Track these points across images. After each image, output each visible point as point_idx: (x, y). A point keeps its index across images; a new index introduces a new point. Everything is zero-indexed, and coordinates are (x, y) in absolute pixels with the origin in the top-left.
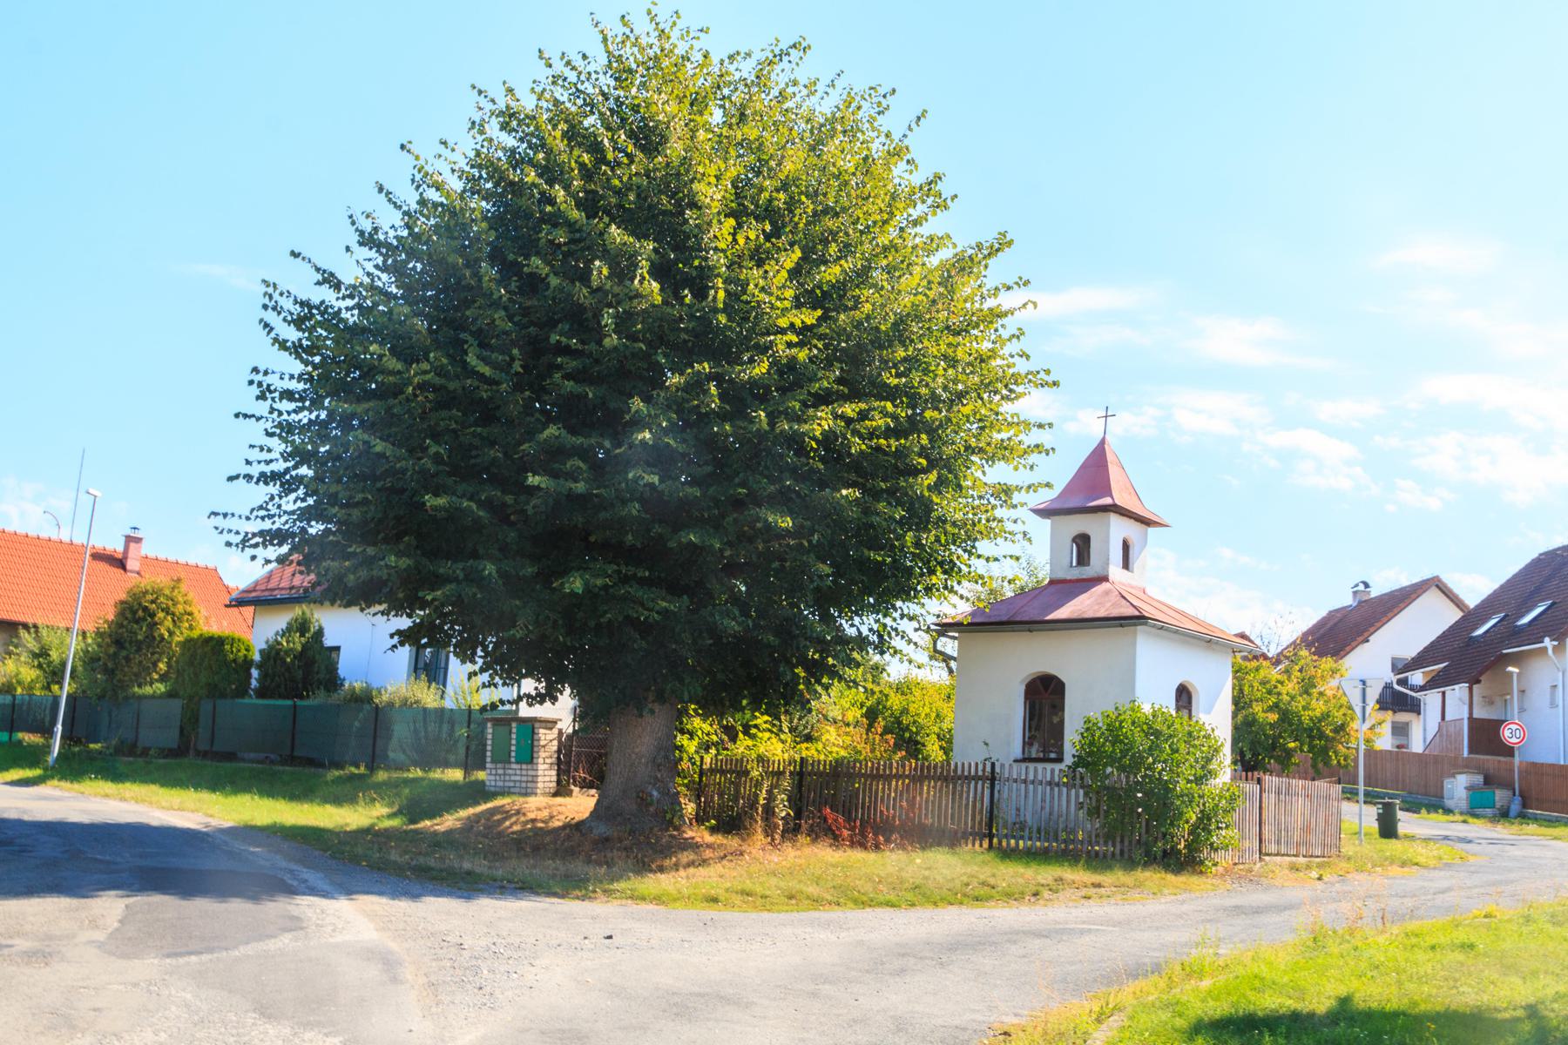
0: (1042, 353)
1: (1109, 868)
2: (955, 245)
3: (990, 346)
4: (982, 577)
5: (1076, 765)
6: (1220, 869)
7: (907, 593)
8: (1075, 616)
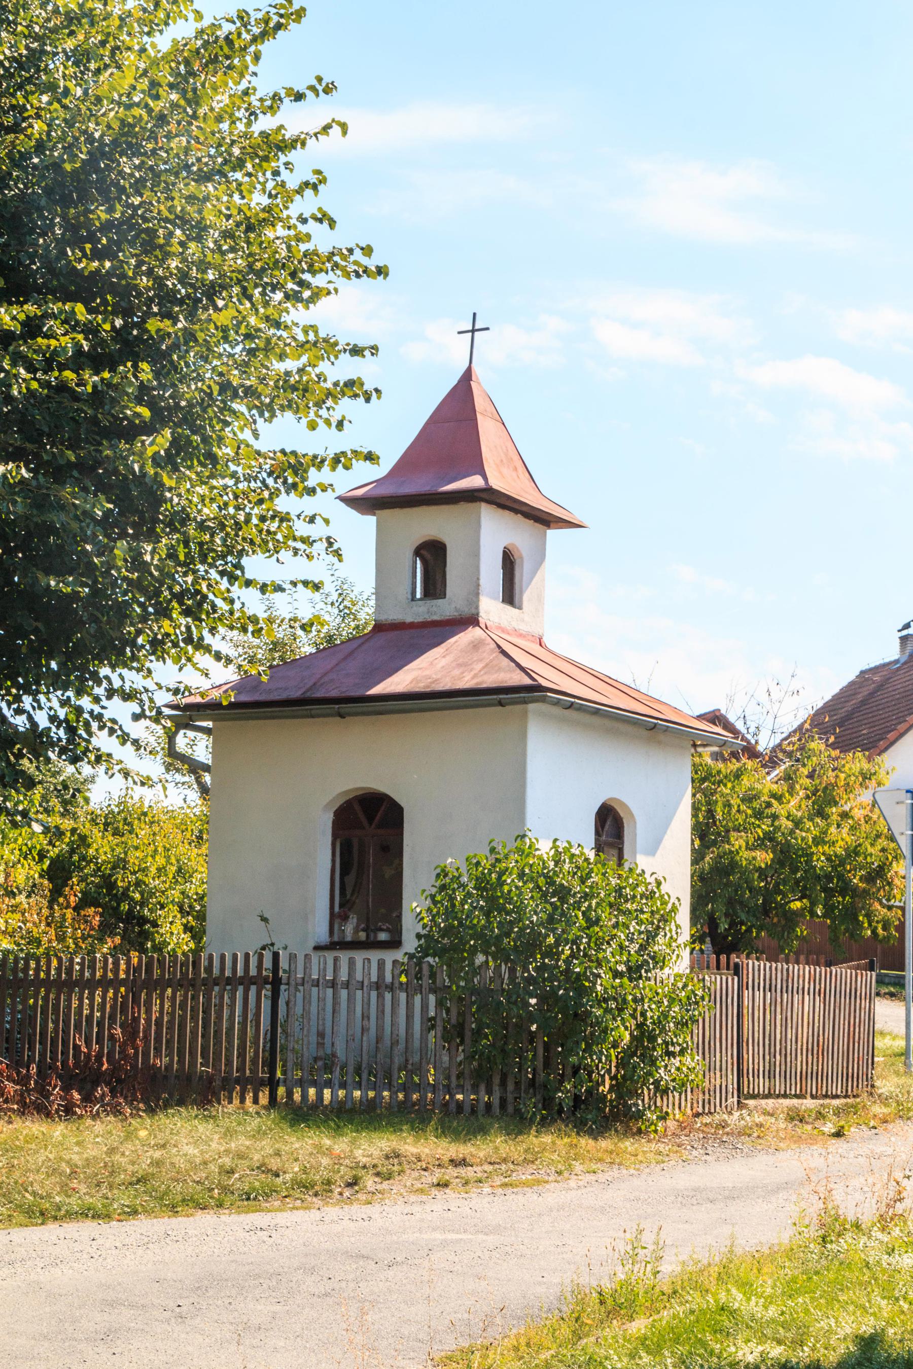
0: (356, 216)
1: (483, 1130)
2: (199, 15)
3: (265, 201)
4: (254, 620)
5: (425, 951)
6: (671, 1124)
7: (118, 651)
8: (420, 687)
